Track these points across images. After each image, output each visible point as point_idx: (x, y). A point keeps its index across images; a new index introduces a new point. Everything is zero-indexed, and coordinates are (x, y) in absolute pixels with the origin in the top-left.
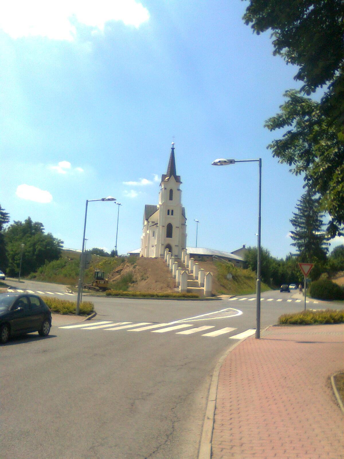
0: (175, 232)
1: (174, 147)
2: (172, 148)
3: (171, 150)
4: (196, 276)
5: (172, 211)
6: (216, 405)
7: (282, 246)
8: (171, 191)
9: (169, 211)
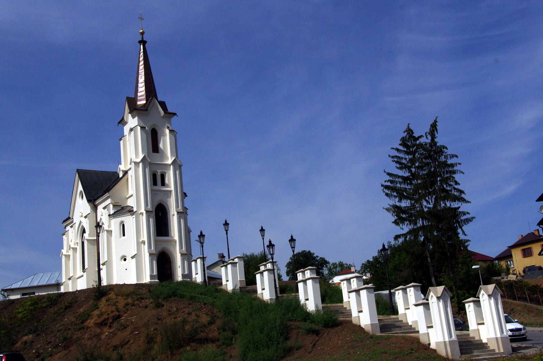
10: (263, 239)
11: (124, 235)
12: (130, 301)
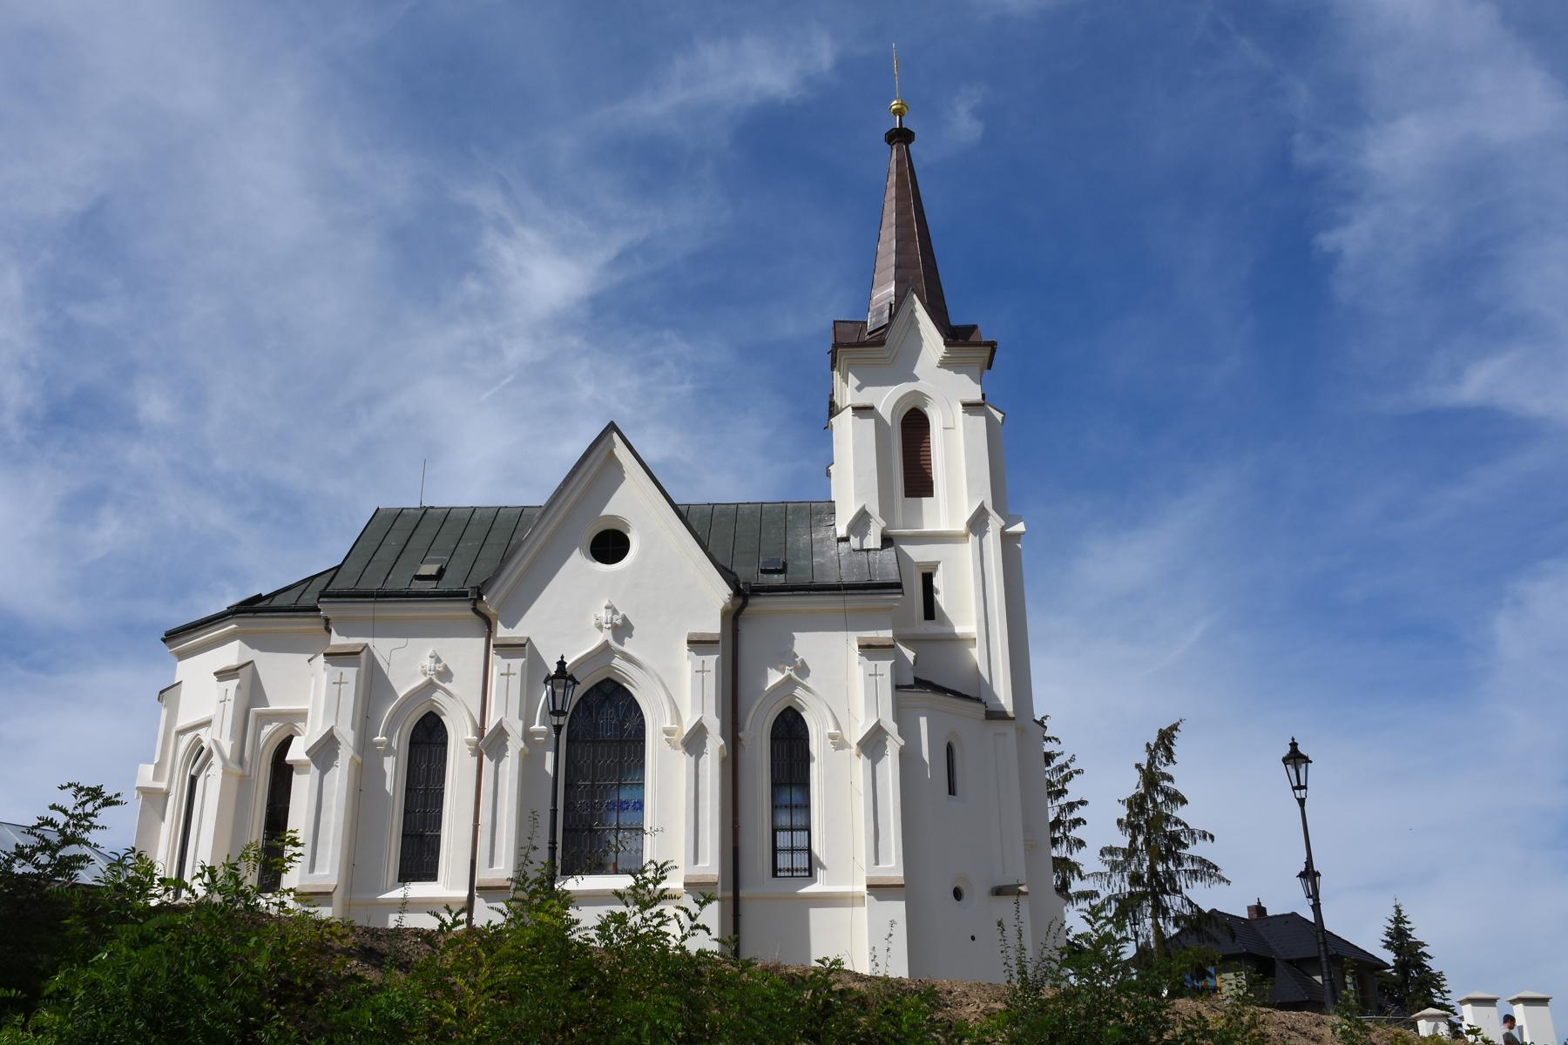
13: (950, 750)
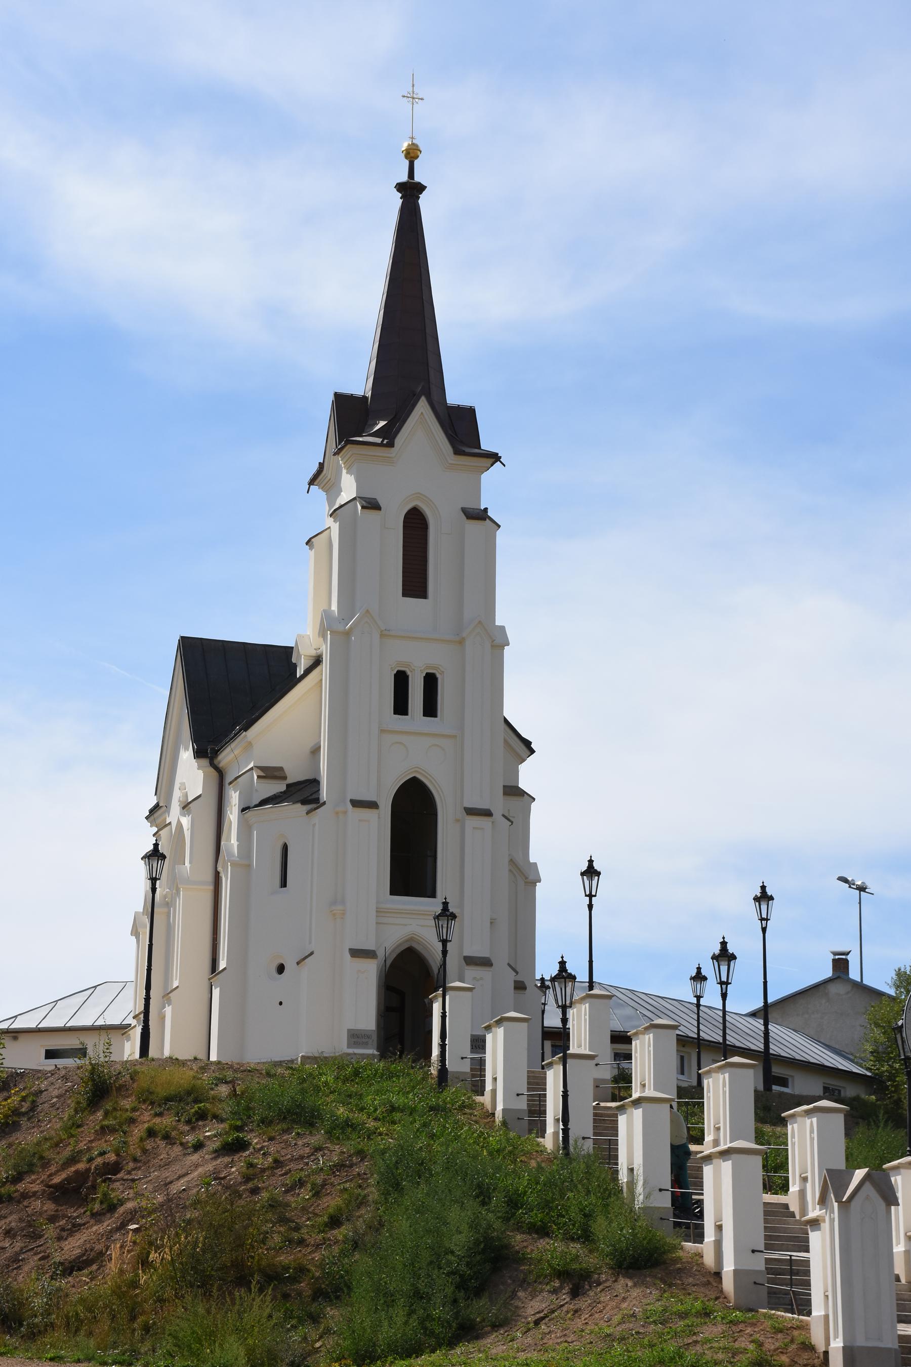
0: (457, 846)
1: (417, 178)
2: (400, 187)
3: (396, 200)
4: (848, 1344)
5: (401, 707)
6: (256, 806)
7: (155, 829)
8: (416, 525)
9: (401, 680)
10: (764, 930)
11: (284, 884)
12: (167, 1121)
13: (285, 848)
